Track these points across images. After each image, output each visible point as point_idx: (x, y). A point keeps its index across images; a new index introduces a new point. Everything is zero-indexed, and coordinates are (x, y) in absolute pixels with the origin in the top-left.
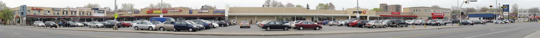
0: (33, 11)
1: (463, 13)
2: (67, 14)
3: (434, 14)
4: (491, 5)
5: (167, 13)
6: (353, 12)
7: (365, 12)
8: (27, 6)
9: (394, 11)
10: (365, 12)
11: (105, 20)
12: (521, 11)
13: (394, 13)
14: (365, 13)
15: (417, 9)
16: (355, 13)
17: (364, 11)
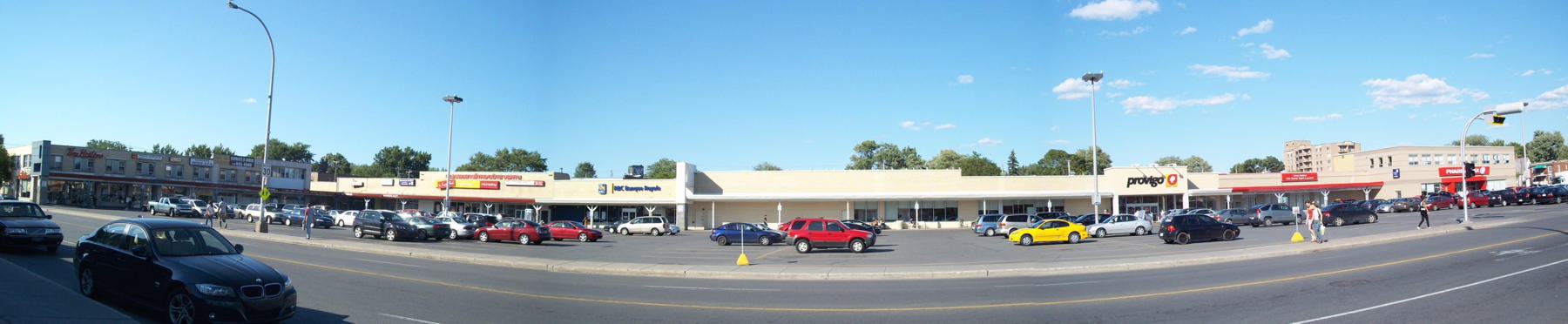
0: (71, 159)
1: (1472, 165)
2: (1461, 168)
3: (1447, 172)
4: (1498, 125)
6: (1129, 179)
7: (1172, 179)
10: (1172, 179)
12: (1498, 162)
13: (1290, 175)
14: (1175, 181)
15: (1390, 154)
16: (1134, 182)
17: (1170, 176)
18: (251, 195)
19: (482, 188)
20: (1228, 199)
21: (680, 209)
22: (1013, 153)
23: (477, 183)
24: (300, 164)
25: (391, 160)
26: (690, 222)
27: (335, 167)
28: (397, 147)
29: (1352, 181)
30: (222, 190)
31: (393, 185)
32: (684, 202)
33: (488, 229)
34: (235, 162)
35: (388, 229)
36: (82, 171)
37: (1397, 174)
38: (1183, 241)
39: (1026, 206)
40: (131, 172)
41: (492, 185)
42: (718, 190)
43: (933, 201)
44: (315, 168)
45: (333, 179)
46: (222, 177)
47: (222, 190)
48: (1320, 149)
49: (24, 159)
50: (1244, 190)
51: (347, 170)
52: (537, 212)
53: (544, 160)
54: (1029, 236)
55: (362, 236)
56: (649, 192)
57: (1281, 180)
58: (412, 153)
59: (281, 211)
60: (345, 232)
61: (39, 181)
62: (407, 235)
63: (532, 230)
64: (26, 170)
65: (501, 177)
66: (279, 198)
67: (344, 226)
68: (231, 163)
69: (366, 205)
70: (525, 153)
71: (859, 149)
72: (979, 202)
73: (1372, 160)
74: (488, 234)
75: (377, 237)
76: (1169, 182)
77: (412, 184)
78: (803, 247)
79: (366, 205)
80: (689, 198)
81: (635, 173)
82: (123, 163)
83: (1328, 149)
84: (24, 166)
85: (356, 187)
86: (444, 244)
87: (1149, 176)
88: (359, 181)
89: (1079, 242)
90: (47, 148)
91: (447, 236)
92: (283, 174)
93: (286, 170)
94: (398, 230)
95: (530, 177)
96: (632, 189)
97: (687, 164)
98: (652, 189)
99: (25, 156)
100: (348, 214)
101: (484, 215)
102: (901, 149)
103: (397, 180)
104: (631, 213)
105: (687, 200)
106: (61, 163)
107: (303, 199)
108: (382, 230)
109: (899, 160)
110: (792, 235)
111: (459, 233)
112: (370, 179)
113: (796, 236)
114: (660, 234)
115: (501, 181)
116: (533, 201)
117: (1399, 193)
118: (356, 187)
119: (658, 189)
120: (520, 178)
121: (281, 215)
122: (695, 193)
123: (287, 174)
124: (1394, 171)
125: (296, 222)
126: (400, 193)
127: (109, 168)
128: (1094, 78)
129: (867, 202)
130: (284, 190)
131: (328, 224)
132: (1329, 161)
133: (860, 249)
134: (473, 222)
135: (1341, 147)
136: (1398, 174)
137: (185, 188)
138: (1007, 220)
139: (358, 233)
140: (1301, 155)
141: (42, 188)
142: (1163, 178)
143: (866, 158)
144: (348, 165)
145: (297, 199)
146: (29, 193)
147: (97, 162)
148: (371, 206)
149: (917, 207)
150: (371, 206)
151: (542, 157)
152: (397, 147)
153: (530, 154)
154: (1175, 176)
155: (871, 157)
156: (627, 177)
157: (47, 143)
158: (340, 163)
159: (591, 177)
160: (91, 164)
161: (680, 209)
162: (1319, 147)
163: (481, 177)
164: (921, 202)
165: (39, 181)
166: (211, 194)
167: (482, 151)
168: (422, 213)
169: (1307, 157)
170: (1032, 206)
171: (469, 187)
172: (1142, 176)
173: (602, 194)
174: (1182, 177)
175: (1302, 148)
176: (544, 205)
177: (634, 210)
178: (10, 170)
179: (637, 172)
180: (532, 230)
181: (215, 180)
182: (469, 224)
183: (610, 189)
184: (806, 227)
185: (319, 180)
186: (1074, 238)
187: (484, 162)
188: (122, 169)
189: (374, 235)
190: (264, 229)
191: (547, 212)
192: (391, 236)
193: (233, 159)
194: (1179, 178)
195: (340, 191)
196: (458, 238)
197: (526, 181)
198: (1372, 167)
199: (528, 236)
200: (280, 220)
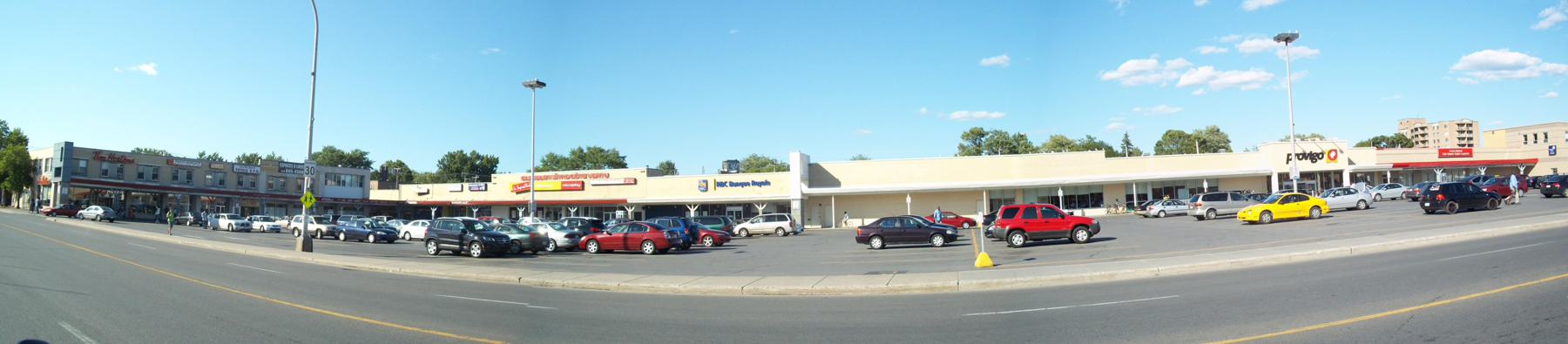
5: (583, 188)
7: (1333, 155)
8: (75, 145)
9: (1452, 143)
11: (317, 235)
13: (1447, 151)
14: (1336, 157)
15: (1545, 130)
17: (1330, 151)
18: (289, 205)
19: (564, 189)
20: (1389, 175)
21: (796, 206)
22: (1126, 136)
23: (557, 184)
24: (360, 171)
25: (456, 166)
26: (806, 221)
27: (395, 175)
28: (462, 152)
29: (1506, 157)
30: (271, 201)
31: (462, 191)
32: (800, 197)
33: (599, 236)
34: (284, 169)
35: (473, 242)
36: (110, 178)
37: (1553, 151)
38: (1452, 211)
39: (1177, 188)
40: (165, 179)
41: (575, 185)
42: (836, 183)
43: (1076, 187)
44: (375, 176)
45: (394, 187)
46: (270, 186)
47: (271, 201)
48: (1438, 127)
49: (46, 164)
50: (1405, 165)
51: (410, 178)
52: (630, 214)
53: (624, 158)
54: (1269, 212)
55: (437, 252)
56: (756, 187)
57: (1437, 155)
58: (478, 157)
59: (336, 223)
60: (412, 250)
61: (59, 187)
62: (498, 249)
63: (658, 235)
64: (47, 175)
65: (585, 176)
66: (327, 208)
67: (411, 239)
68: (280, 170)
69: (433, 214)
70: (602, 151)
71: (966, 136)
72: (1127, 185)
73: (1526, 136)
74: (598, 242)
75: (457, 253)
76: (1329, 157)
77: (484, 188)
78: (1018, 239)
79: (433, 214)
80: (805, 192)
81: (730, 168)
82: (157, 169)
83: (1445, 127)
84: (46, 171)
85: (420, 194)
86: (541, 259)
87: (1308, 152)
88: (424, 188)
89: (1320, 217)
90: (69, 150)
91: (543, 248)
92: (339, 182)
93: (343, 177)
94: (486, 243)
95: (617, 175)
96: (737, 185)
97: (801, 154)
98: (760, 184)
99: (47, 160)
100: (414, 224)
101: (587, 218)
102: (1011, 134)
103: (466, 185)
104: (737, 212)
105: (803, 194)
106: (85, 169)
107: (362, 209)
108: (461, 244)
109: (1013, 146)
110: (1003, 225)
111: (559, 244)
112: (435, 185)
113: (1007, 228)
114: (786, 234)
115: (585, 181)
116: (625, 201)
117: (1555, 170)
118: (420, 194)
119: (767, 183)
120: (608, 176)
121: (334, 228)
122: (810, 186)
123: (344, 182)
124: (1550, 147)
125: (352, 236)
126: (470, 200)
127: (141, 176)
128: (1288, 39)
129: (1003, 190)
130: (341, 199)
131: (390, 237)
132: (1447, 140)
133: (1085, 238)
134: (573, 228)
135: (1458, 125)
136: (1555, 151)
137: (228, 199)
138: (1203, 200)
139: (432, 248)
140: (1417, 133)
141: (62, 196)
142: (1322, 154)
143: (975, 146)
144: (410, 172)
145: (355, 209)
146: (48, 201)
147: (127, 167)
148: (438, 214)
149: (1060, 193)
150: (438, 214)
151: (621, 155)
152: (462, 152)
153: (608, 151)
154: (1336, 151)
155: (979, 145)
156: (723, 173)
157: (69, 145)
158: (401, 171)
159: (673, 174)
160: (120, 170)
161: (796, 206)
162: (1435, 125)
163: (562, 177)
164: (1064, 188)
165: (59, 187)
166: (257, 205)
167: (553, 152)
168: (500, 220)
169: (1423, 135)
170: (1183, 187)
171: (550, 189)
172: (1301, 152)
173: (703, 191)
174: (1341, 152)
175: (1418, 125)
176: (637, 205)
177: (740, 209)
178: (32, 175)
179: (732, 166)
180: (658, 235)
181: (262, 189)
182: (570, 231)
183: (711, 185)
184: (1019, 215)
185: (380, 188)
186: (1316, 213)
187: (558, 162)
188: (155, 176)
189: (453, 250)
190: (308, 247)
191: (640, 213)
192: (476, 250)
193: (282, 165)
194: (1339, 153)
195: (403, 199)
196: (558, 250)
197: (615, 179)
198: (1536, 142)
199: (654, 243)
200: (333, 234)
